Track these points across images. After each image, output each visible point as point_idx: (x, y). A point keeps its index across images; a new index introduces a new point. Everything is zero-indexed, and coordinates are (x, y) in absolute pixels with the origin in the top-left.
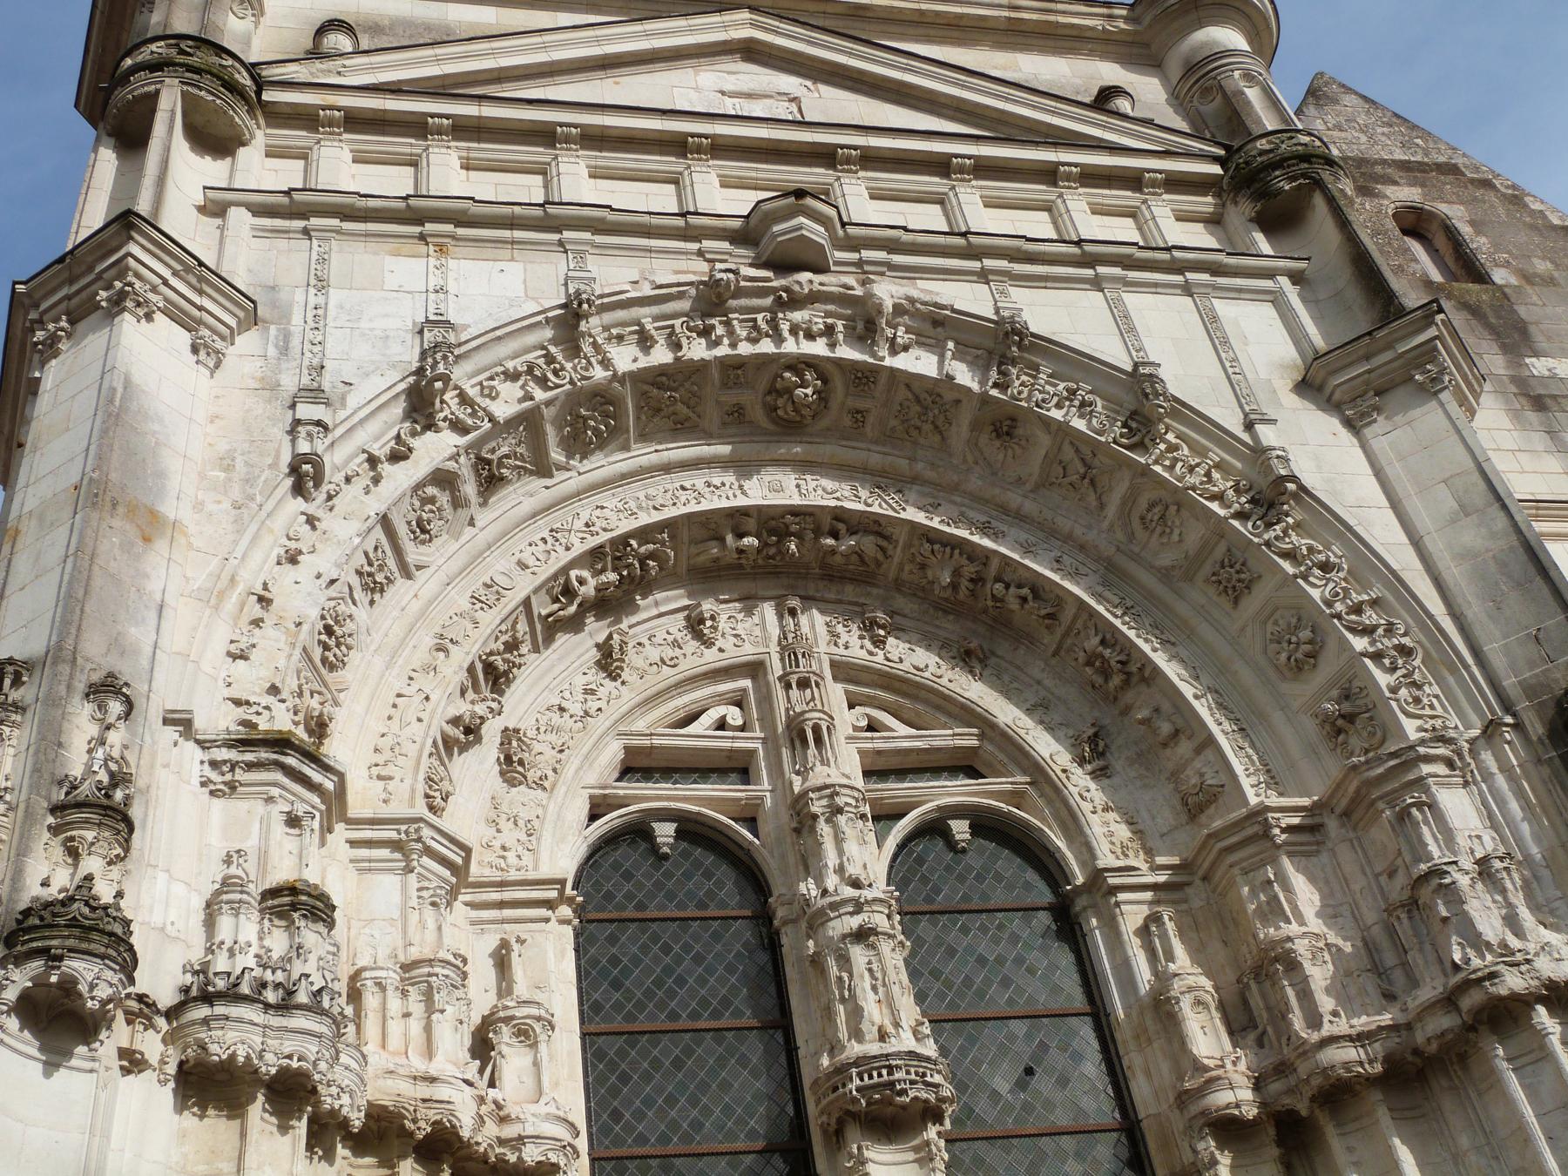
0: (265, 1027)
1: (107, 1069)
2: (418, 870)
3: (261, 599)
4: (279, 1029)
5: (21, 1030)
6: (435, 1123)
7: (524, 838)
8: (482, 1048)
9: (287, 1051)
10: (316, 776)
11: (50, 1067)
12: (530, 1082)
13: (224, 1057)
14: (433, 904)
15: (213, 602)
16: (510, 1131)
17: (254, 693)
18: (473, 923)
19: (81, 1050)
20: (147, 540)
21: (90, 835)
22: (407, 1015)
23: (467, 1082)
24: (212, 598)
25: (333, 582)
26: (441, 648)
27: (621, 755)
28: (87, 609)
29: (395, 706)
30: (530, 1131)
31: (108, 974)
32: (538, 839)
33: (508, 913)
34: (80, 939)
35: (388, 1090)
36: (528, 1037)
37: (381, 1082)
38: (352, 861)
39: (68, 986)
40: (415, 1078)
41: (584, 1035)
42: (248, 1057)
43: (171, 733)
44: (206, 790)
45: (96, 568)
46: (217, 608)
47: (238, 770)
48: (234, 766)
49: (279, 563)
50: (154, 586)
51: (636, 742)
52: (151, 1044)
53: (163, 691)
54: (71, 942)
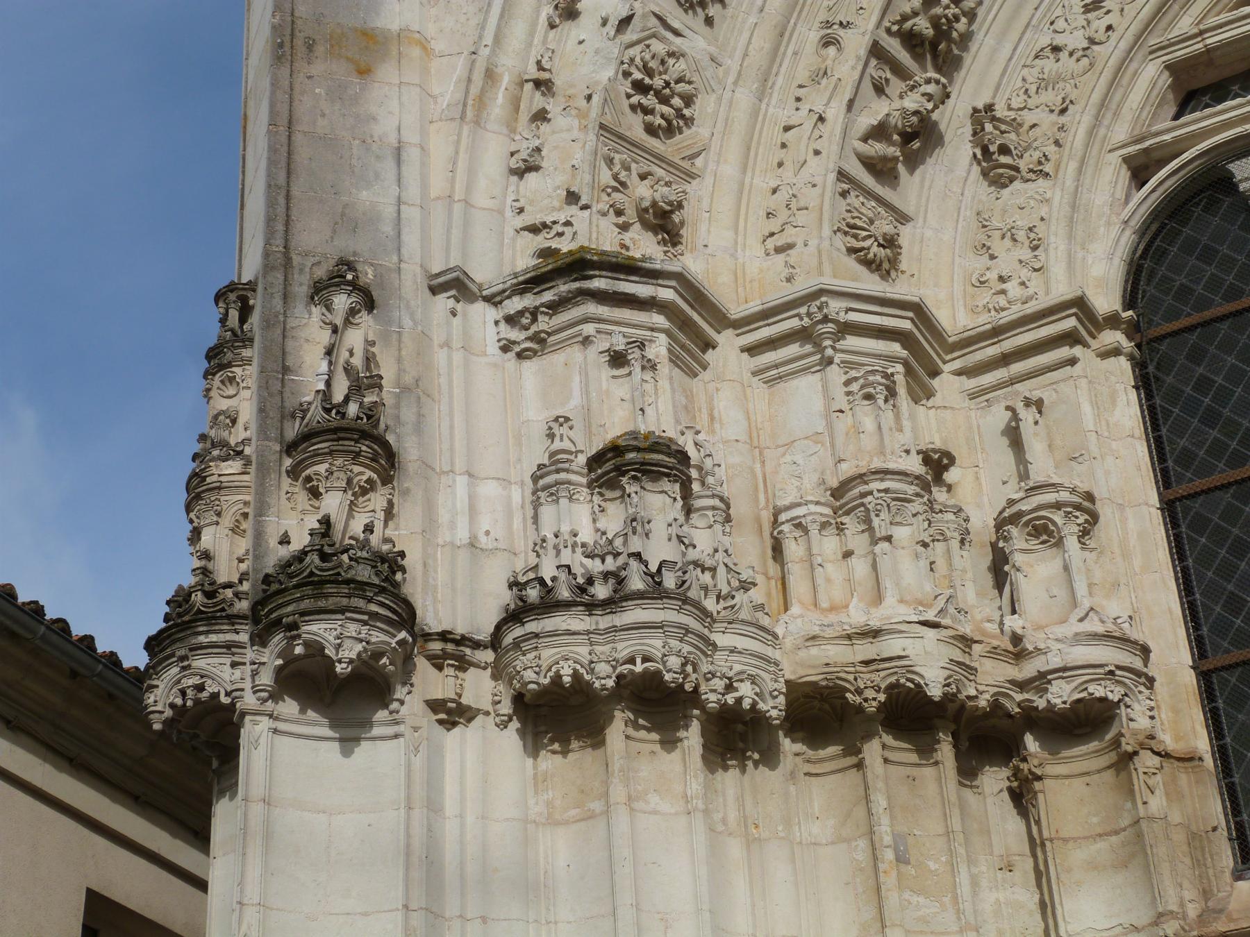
0: (588, 632)
1: (416, 729)
2: (838, 358)
3: (538, 84)
4: (607, 631)
5: (303, 711)
6: (891, 687)
7: (1026, 254)
8: (1000, 570)
9: (623, 654)
10: (642, 290)
11: (348, 743)
12: (1061, 593)
13: (547, 681)
14: (868, 397)
15: (470, 114)
16: (1029, 669)
17: (554, 209)
18: (973, 396)
19: (382, 715)
20: (364, 72)
21: (322, 468)
22: (848, 554)
23: (925, 623)
24: (470, 110)
25: (625, 22)
26: (828, 42)
27: (1166, 80)
28: (295, 192)
29: (784, 146)
30: (1055, 661)
31: (352, 629)
32: (1046, 250)
33: (1018, 368)
34: (316, 597)
35: (803, 661)
36: (1050, 534)
37: (802, 654)
38: (754, 374)
39: (316, 649)
40: (849, 637)
41: (1170, 509)
42: (576, 675)
43: (444, 302)
44: (511, 355)
45: (298, 138)
46: (477, 122)
47: (540, 318)
48: (534, 313)
49: (552, 26)
50: (385, 128)
51: (1181, 53)
52: (478, 687)
53: (422, 250)
54: (306, 604)
